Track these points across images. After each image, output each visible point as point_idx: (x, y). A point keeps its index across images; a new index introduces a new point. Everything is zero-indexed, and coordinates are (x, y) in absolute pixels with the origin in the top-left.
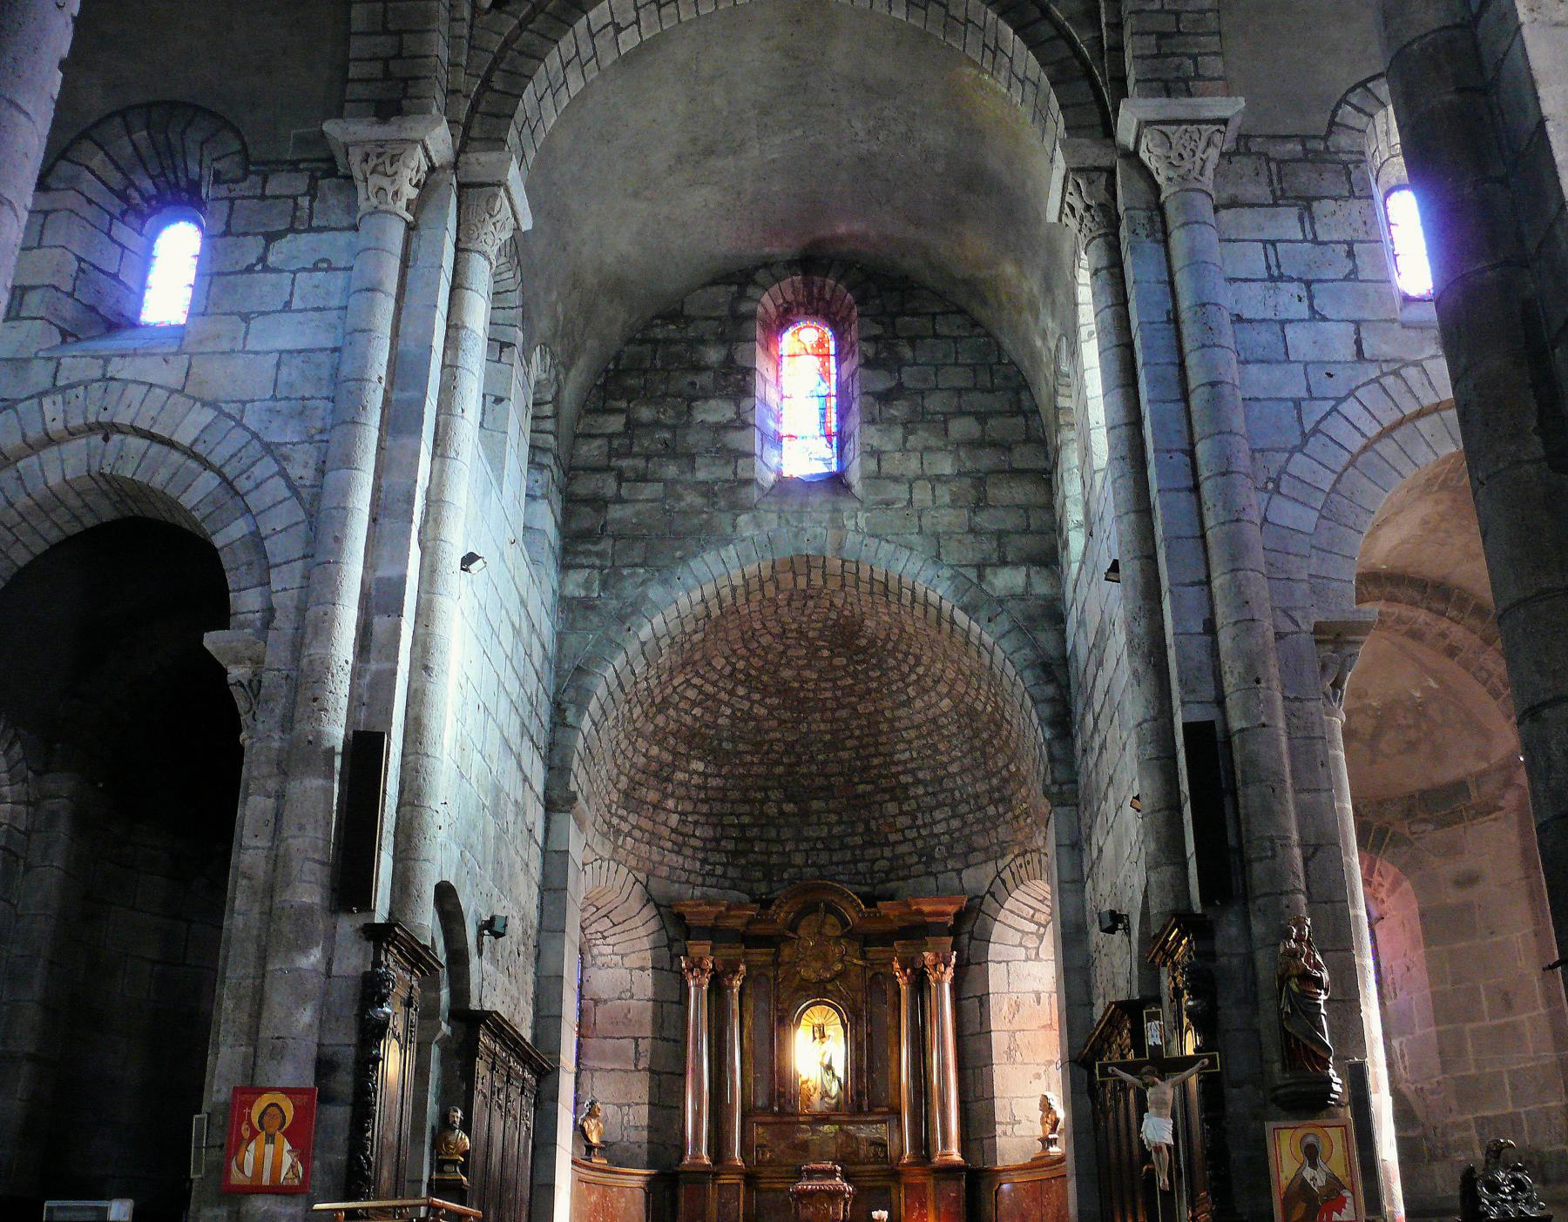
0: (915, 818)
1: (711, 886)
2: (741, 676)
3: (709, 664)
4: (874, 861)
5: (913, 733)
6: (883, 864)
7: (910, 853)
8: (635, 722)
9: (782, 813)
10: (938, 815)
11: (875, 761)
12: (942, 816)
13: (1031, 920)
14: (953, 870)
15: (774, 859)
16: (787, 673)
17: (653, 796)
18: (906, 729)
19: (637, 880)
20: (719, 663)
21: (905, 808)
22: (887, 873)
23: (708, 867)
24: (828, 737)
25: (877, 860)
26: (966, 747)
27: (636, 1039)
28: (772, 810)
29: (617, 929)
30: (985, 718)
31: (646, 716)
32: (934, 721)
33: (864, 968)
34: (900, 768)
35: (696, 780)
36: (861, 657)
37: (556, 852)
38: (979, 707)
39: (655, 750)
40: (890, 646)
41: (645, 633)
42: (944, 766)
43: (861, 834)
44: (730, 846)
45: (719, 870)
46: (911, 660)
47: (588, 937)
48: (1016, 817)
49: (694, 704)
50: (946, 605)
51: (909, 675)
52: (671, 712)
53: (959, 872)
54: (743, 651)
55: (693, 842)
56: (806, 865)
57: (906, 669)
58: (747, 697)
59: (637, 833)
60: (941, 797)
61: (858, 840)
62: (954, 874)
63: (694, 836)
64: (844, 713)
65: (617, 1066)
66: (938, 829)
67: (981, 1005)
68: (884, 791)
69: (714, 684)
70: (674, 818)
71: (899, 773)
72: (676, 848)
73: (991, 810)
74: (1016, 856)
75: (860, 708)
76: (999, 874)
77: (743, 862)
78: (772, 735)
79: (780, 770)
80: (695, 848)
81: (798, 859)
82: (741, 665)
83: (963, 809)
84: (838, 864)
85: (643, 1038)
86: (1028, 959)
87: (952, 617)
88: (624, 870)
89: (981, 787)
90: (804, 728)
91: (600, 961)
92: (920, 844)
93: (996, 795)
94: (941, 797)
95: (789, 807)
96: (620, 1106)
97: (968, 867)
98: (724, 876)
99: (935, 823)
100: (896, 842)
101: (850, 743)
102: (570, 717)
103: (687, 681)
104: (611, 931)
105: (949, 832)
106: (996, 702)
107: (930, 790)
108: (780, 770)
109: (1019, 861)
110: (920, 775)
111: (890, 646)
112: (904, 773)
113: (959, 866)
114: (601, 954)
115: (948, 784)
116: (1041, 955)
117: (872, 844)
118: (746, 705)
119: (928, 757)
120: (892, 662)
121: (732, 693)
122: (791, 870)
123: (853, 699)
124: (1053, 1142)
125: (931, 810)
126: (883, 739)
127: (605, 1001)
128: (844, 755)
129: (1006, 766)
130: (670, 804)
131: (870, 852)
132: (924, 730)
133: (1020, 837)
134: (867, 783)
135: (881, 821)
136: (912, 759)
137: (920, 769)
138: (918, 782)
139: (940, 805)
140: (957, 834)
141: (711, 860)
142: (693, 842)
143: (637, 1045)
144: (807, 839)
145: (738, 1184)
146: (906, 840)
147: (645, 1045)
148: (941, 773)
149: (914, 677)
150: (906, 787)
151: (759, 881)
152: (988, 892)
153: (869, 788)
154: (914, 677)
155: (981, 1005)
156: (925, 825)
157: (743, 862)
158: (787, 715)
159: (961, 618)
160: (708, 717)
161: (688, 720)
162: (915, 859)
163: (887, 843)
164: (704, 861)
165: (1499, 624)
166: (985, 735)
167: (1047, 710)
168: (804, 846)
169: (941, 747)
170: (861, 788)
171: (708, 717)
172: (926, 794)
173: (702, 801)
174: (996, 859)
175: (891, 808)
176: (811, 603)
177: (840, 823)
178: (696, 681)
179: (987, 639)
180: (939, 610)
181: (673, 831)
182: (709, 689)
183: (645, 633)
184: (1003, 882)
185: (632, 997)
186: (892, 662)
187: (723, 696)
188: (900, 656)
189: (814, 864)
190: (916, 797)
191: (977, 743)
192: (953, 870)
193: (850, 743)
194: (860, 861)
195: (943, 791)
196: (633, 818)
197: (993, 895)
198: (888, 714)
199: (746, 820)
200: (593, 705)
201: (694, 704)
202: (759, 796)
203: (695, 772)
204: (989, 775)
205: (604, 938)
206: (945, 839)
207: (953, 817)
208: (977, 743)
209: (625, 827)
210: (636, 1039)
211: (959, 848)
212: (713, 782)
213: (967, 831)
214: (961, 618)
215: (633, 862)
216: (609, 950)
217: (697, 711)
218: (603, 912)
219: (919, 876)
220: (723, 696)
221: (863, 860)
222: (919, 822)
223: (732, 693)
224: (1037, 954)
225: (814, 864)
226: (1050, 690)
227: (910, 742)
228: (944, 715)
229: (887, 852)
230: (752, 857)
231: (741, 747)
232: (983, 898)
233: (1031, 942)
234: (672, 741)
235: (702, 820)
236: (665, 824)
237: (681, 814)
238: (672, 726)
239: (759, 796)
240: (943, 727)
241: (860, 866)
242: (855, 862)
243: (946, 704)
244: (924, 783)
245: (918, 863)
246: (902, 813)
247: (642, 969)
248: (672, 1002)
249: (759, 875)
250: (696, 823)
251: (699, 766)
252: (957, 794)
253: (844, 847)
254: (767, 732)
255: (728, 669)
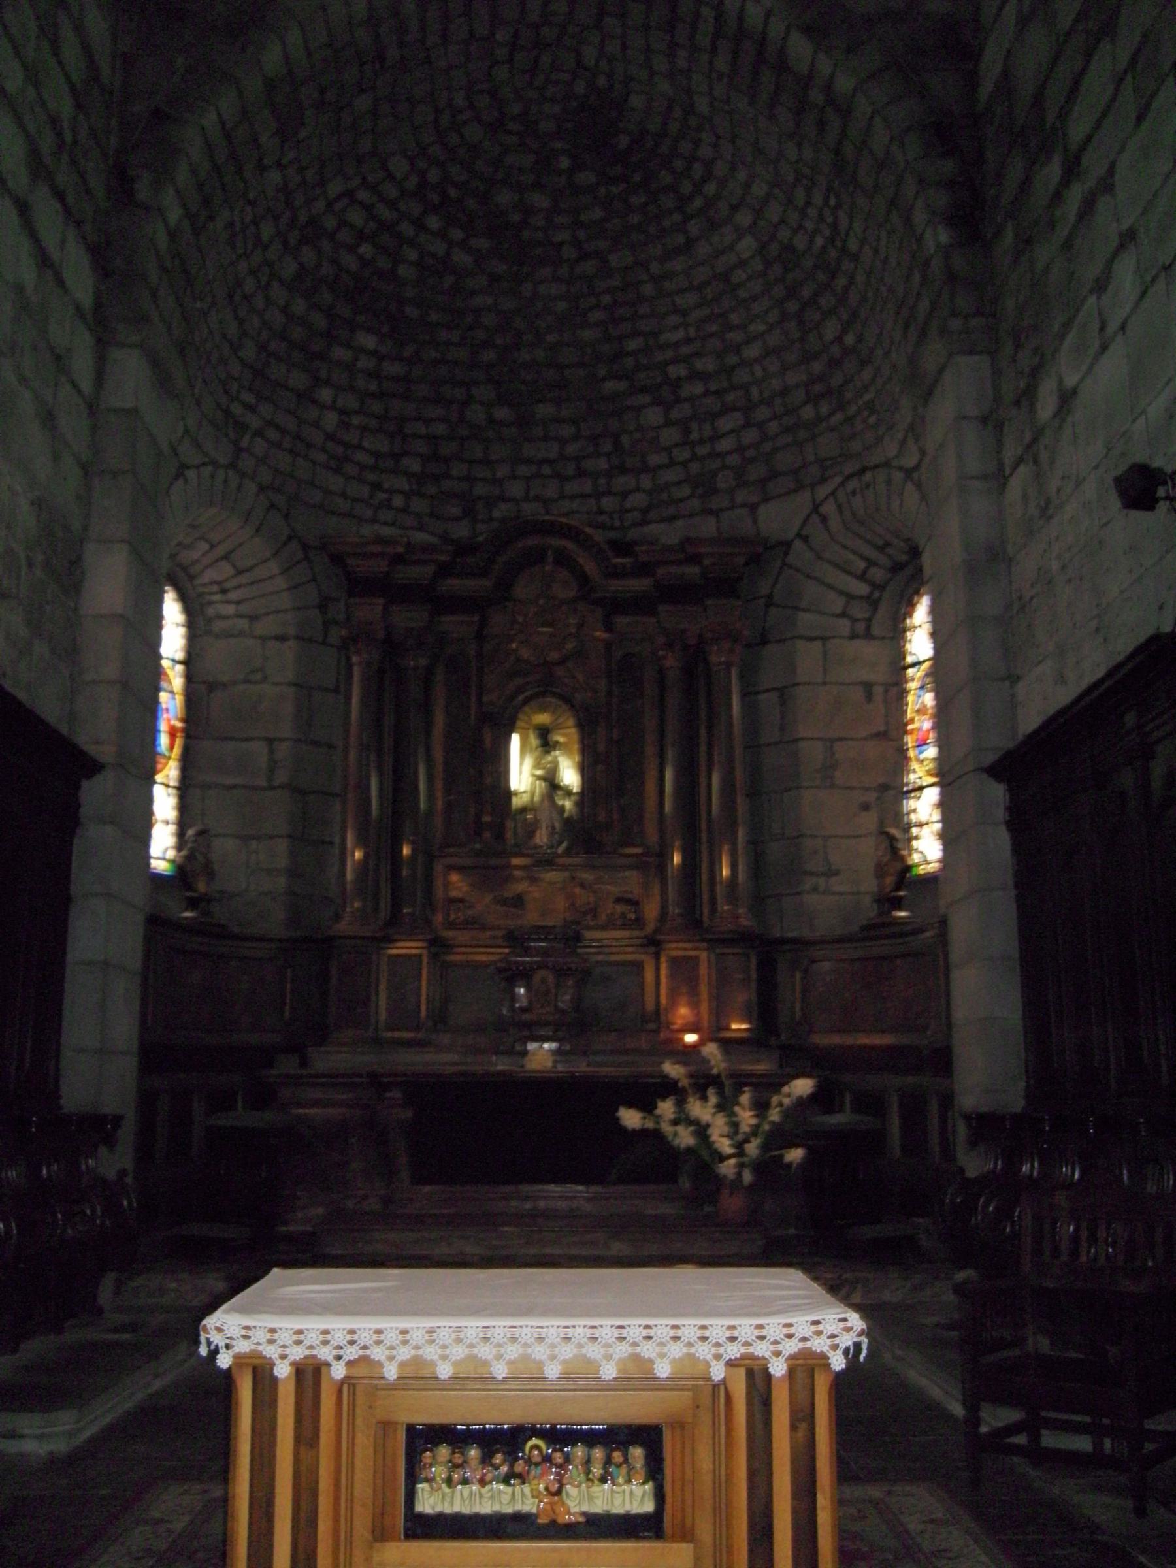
0: (687, 431)
1: (385, 523)
2: (435, 198)
3: (384, 167)
4: (625, 495)
5: (691, 299)
6: (637, 500)
7: (679, 483)
8: (266, 247)
9: (491, 420)
10: (726, 423)
11: (632, 345)
12: (728, 427)
13: (862, 577)
14: (744, 505)
15: (480, 490)
16: (504, 198)
17: (299, 380)
18: (680, 292)
19: (273, 506)
20: (398, 166)
21: (675, 414)
22: (645, 511)
23: (382, 496)
24: (562, 306)
25: (630, 492)
26: (774, 315)
27: (270, 741)
28: (476, 414)
29: (244, 579)
30: (808, 263)
31: (285, 243)
32: (725, 277)
33: (608, 645)
34: (669, 354)
35: (364, 363)
36: (618, 169)
37: (116, 411)
38: (800, 242)
39: (299, 306)
40: (664, 149)
41: (272, 59)
42: (737, 349)
43: (608, 455)
44: (415, 466)
45: (398, 501)
46: (698, 170)
47: (200, 590)
48: (849, 420)
49: (361, 237)
50: (776, 29)
51: (691, 198)
52: (326, 245)
53: (753, 508)
54: (436, 151)
55: (360, 456)
56: (526, 499)
57: (686, 188)
58: (442, 235)
59: (273, 435)
60: (730, 398)
61: (603, 464)
62: (744, 511)
63: (359, 447)
64: (589, 267)
65: (238, 781)
66: (725, 445)
67: (783, 703)
68: (643, 390)
69: (392, 204)
70: (331, 420)
71: (667, 363)
72: (333, 464)
73: (808, 412)
74: (849, 477)
75: (614, 260)
76: (816, 508)
77: (432, 490)
78: (478, 301)
79: (489, 356)
80: (363, 467)
81: (516, 489)
82: (434, 175)
83: (762, 413)
84: (573, 497)
85: (282, 740)
86: (853, 636)
87: (782, 52)
88: (251, 487)
89: (792, 378)
90: (527, 289)
91: (218, 626)
92: (695, 467)
93: (817, 388)
94: (730, 398)
95: (502, 413)
96: (245, 839)
97: (766, 500)
98: (405, 510)
99: (716, 437)
100: (660, 467)
101: (596, 316)
102: (143, 191)
103: (350, 194)
104: (234, 582)
105: (740, 449)
106: (835, 226)
107: (713, 387)
108: (489, 356)
109: (853, 484)
110: (699, 365)
111: (664, 149)
112: (675, 361)
113: (754, 499)
114: (219, 617)
115: (742, 376)
116: (876, 630)
117: (623, 470)
118: (439, 248)
119: (712, 335)
120: (666, 178)
121: (420, 225)
122: (503, 506)
123: (602, 245)
124: (898, 904)
125: (715, 416)
126: (644, 309)
127: (225, 686)
128: (587, 335)
129: (839, 339)
130: (325, 395)
131: (622, 482)
132: (709, 292)
133: (856, 446)
134: (620, 378)
135: (637, 436)
136: (688, 341)
137: (697, 354)
138: (695, 375)
139: (726, 410)
140: (751, 453)
141: (386, 486)
142: (360, 456)
143: (271, 752)
144: (528, 461)
145: (420, 956)
146: (672, 463)
147: (283, 750)
148: (732, 360)
149: (698, 202)
150: (676, 384)
151: (457, 519)
152: (799, 535)
153: (622, 386)
154: (698, 202)
155: (783, 703)
156: (701, 441)
157: (432, 490)
158: (501, 268)
159: (800, 48)
160: (383, 263)
161: (350, 261)
162: (686, 491)
163: (645, 468)
164: (376, 486)
165: (1048, 498)
166: (806, 292)
167: (941, 199)
168: (523, 470)
169: (734, 318)
170: (610, 386)
171: (383, 263)
172: (706, 393)
173: (373, 395)
174: (813, 486)
175: (653, 416)
176: (546, 59)
177: (577, 437)
178: (363, 195)
179: (844, 84)
180: (763, 39)
181: (330, 437)
182: (385, 213)
183: (272, 59)
184: (824, 519)
185: (265, 679)
186: (666, 178)
187: (407, 229)
188: (679, 164)
189: (537, 498)
190: (691, 399)
191: (792, 306)
192: (744, 505)
193: (596, 316)
194: (603, 494)
195: (733, 388)
196: (266, 410)
197: (806, 539)
198: (655, 268)
199: (440, 429)
200: (182, 175)
201: (361, 237)
202: (459, 393)
203: (363, 350)
204: (808, 358)
205: (224, 591)
206: (734, 460)
207: (747, 425)
208: (792, 306)
209: (254, 422)
210: (270, 741)
211: (756, 472)
212: (393, 368)
213: (767, 447)
214: (800, 48)
215: (265, 476)
216: (230, 609)
217: (366, 249)
218: (221, 550)
219: (691, 516)
220: (407, 229)
221: (609, 493)
222: (695, 436)
223: (420, 225)
224: (868, 628)
225: (537, 498)
226: (948, 167)
227: (684, 313)
228: (742, 264)
229: (646, 482)
230: (447, 485)
231: (434, 317)
232: (787, 545)
233: (859, 611)
234: (327, 297)
235: (374, 423)
236: (316, 425)
237: (343, 412)
238: (327, 270)
239: (459, 393)
240: (739, 285)
241: (607, 503)
242: (598, 496)
243: (747, 245)
244: (704, 376)
245: (692, 496)
246: (669, 423)
247: (282, 638)
248: (327, 690)
249: (455, 510)
250: (364, 429)
251: (369, 341)
252: (755, 391)
253: (581, 473)
254: (473, 293)
255: (412, 183)
